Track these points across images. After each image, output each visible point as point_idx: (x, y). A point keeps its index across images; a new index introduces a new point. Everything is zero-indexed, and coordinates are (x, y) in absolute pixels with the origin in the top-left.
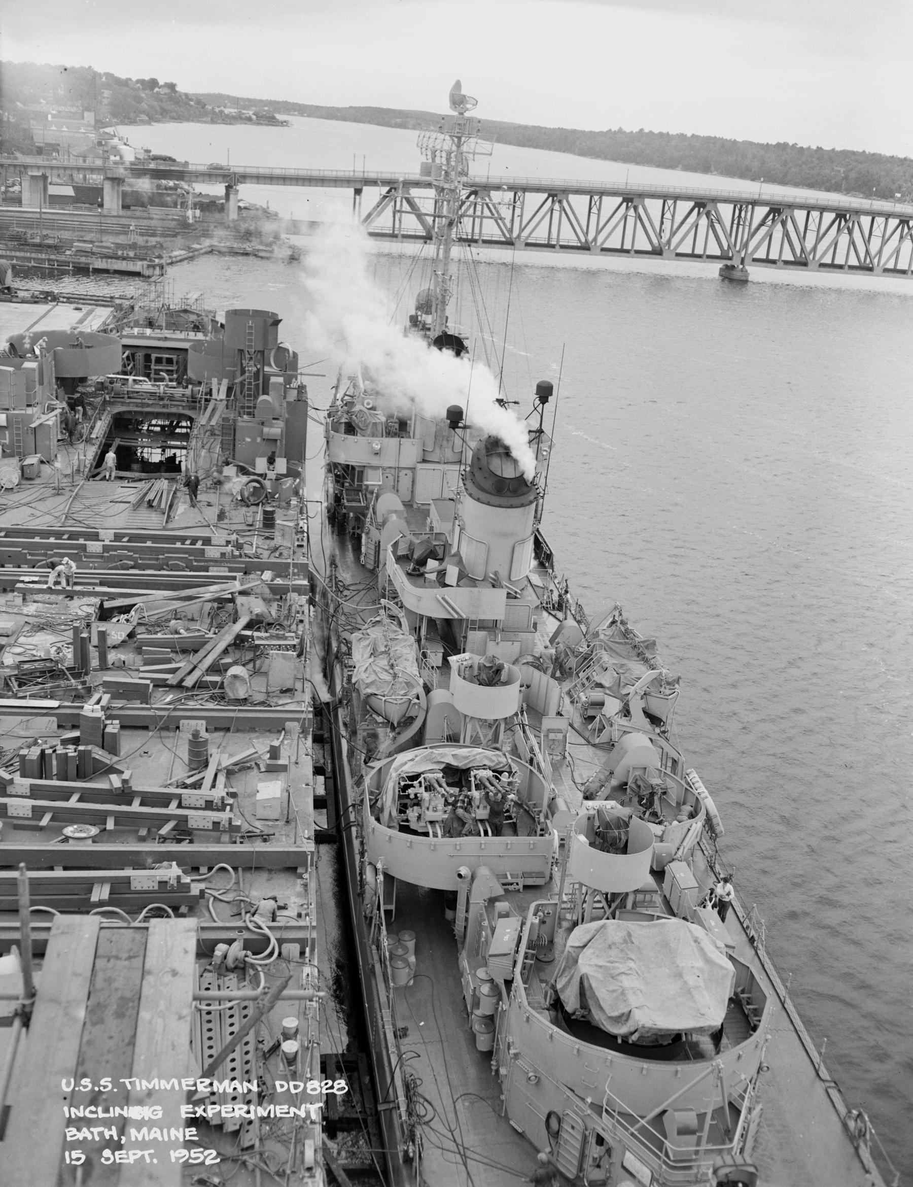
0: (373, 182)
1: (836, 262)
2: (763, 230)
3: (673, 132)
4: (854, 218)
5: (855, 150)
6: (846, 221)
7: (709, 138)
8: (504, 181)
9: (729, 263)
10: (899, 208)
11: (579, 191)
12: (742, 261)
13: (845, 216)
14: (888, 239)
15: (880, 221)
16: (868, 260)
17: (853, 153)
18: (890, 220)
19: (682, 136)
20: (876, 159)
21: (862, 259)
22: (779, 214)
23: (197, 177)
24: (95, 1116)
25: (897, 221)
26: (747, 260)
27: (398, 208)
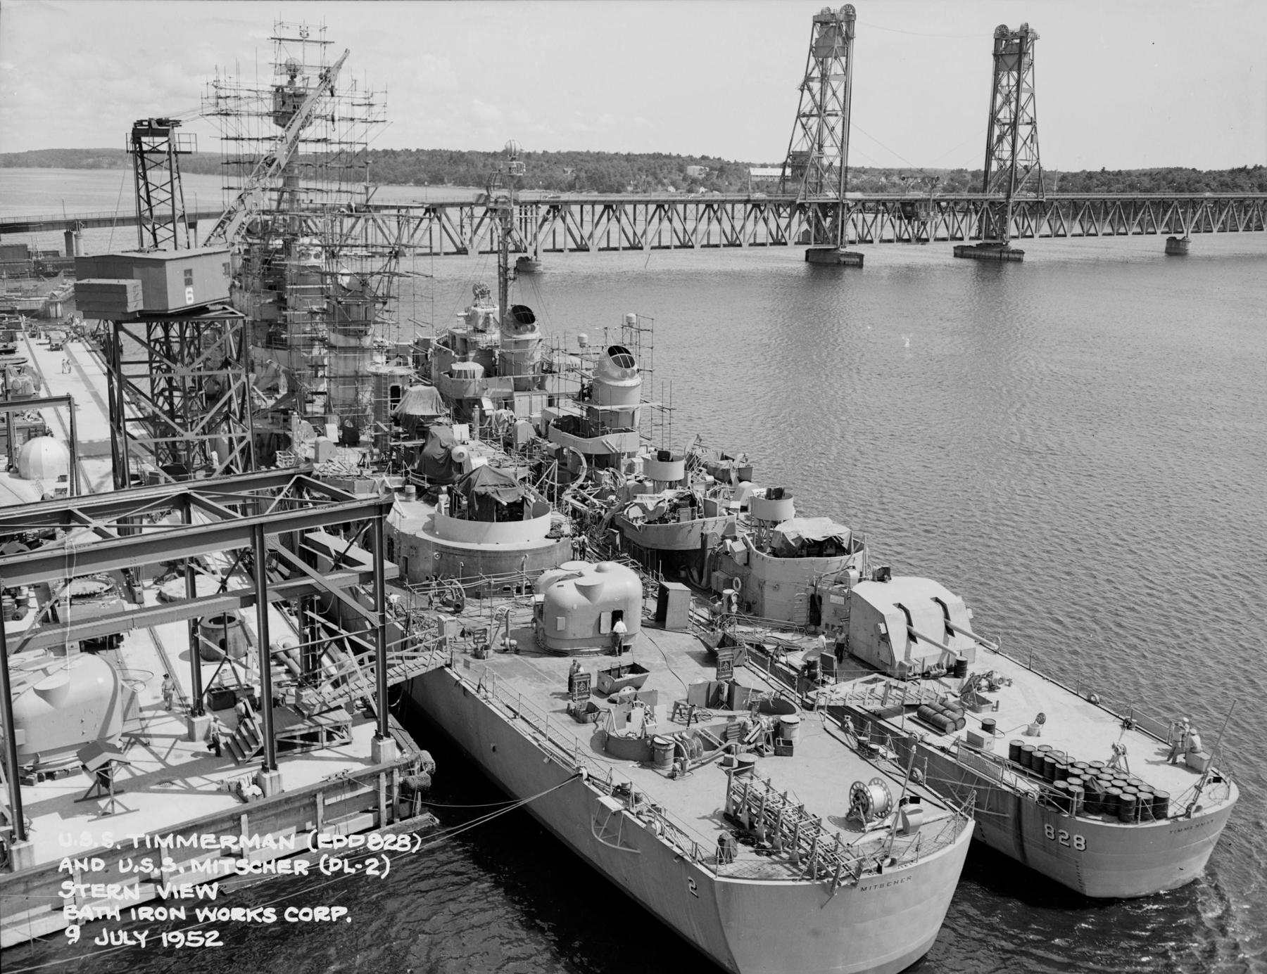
0: (208, 216)
1: (611, 246)
2: (546, 226)
3: (398, 148)
4: (620, 207)
5: (580, 150)
6: (614, 211)
7: (434, 151)
8: (78, 217)
9: (524, 255)
10: (654, 196)
11: (452, 205)
12: (535, 253)
13: (611, 207)
14: (635, 219)
15: (587, 208)
16: (687, 239)
17: (579, 154)
18: (649, 206)
19: (407, 152)
20: (599, 157)
21: (632, 240)
22: (559, 211)
23: (908, 211)
24: (295, 920)
25: (602, 207)
26: (539, 252)
27: (428, 250)
